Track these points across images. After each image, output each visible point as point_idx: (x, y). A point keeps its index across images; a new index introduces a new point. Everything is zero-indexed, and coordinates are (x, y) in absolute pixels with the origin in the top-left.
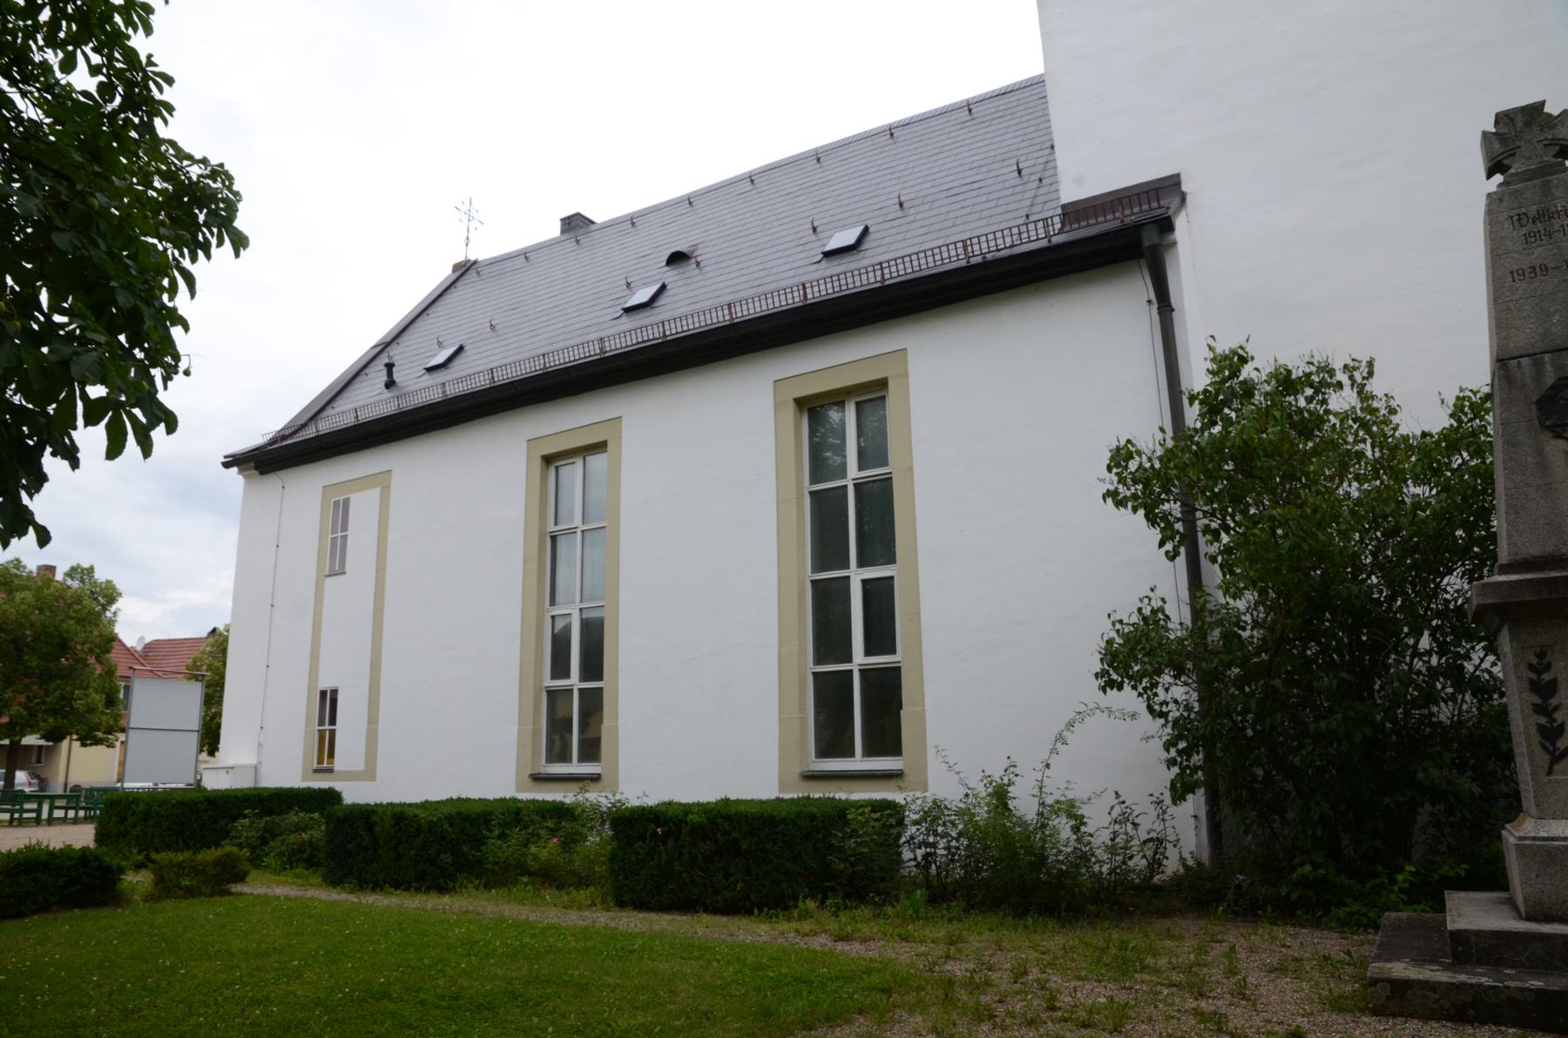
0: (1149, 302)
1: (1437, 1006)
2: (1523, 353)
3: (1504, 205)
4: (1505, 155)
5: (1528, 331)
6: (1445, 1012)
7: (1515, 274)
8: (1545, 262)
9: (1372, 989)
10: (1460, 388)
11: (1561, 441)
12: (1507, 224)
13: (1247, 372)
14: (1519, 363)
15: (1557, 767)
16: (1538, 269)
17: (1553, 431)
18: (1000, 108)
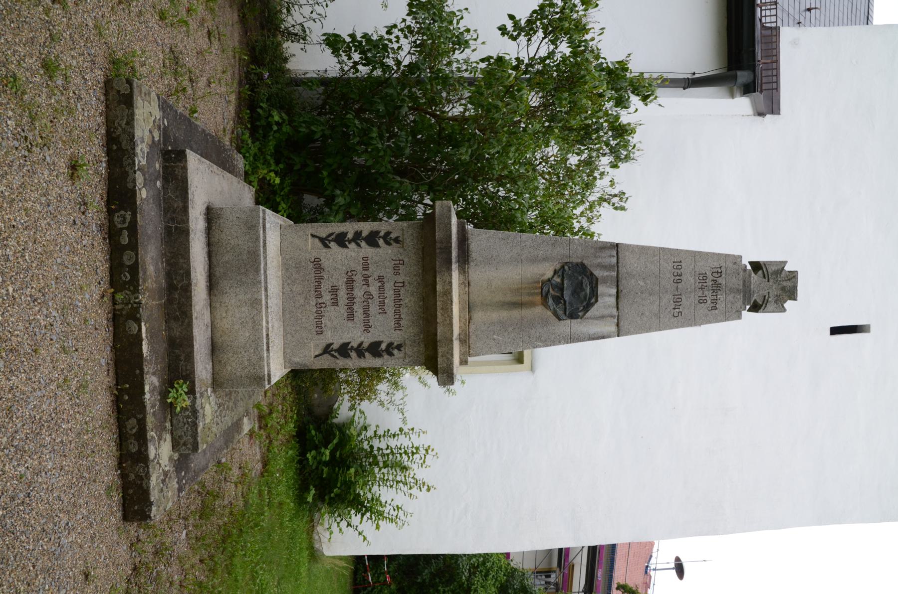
0: (694, 74)
1: (116, 125)
2: (620, 260)
3: (731, 265)
4: (766, 272)
5: (636, 265)
6: (112, 130)
7: (679, 264)
8: (683, 283)
9: (125, 81)
10: (601, 235)
11: (552, 273)
12: (716, 264)
13: (635, 100)
14: (614, 256)
15: (317, 240)
16: (679, 278)
17: (560, 270)
18: (858, 12)
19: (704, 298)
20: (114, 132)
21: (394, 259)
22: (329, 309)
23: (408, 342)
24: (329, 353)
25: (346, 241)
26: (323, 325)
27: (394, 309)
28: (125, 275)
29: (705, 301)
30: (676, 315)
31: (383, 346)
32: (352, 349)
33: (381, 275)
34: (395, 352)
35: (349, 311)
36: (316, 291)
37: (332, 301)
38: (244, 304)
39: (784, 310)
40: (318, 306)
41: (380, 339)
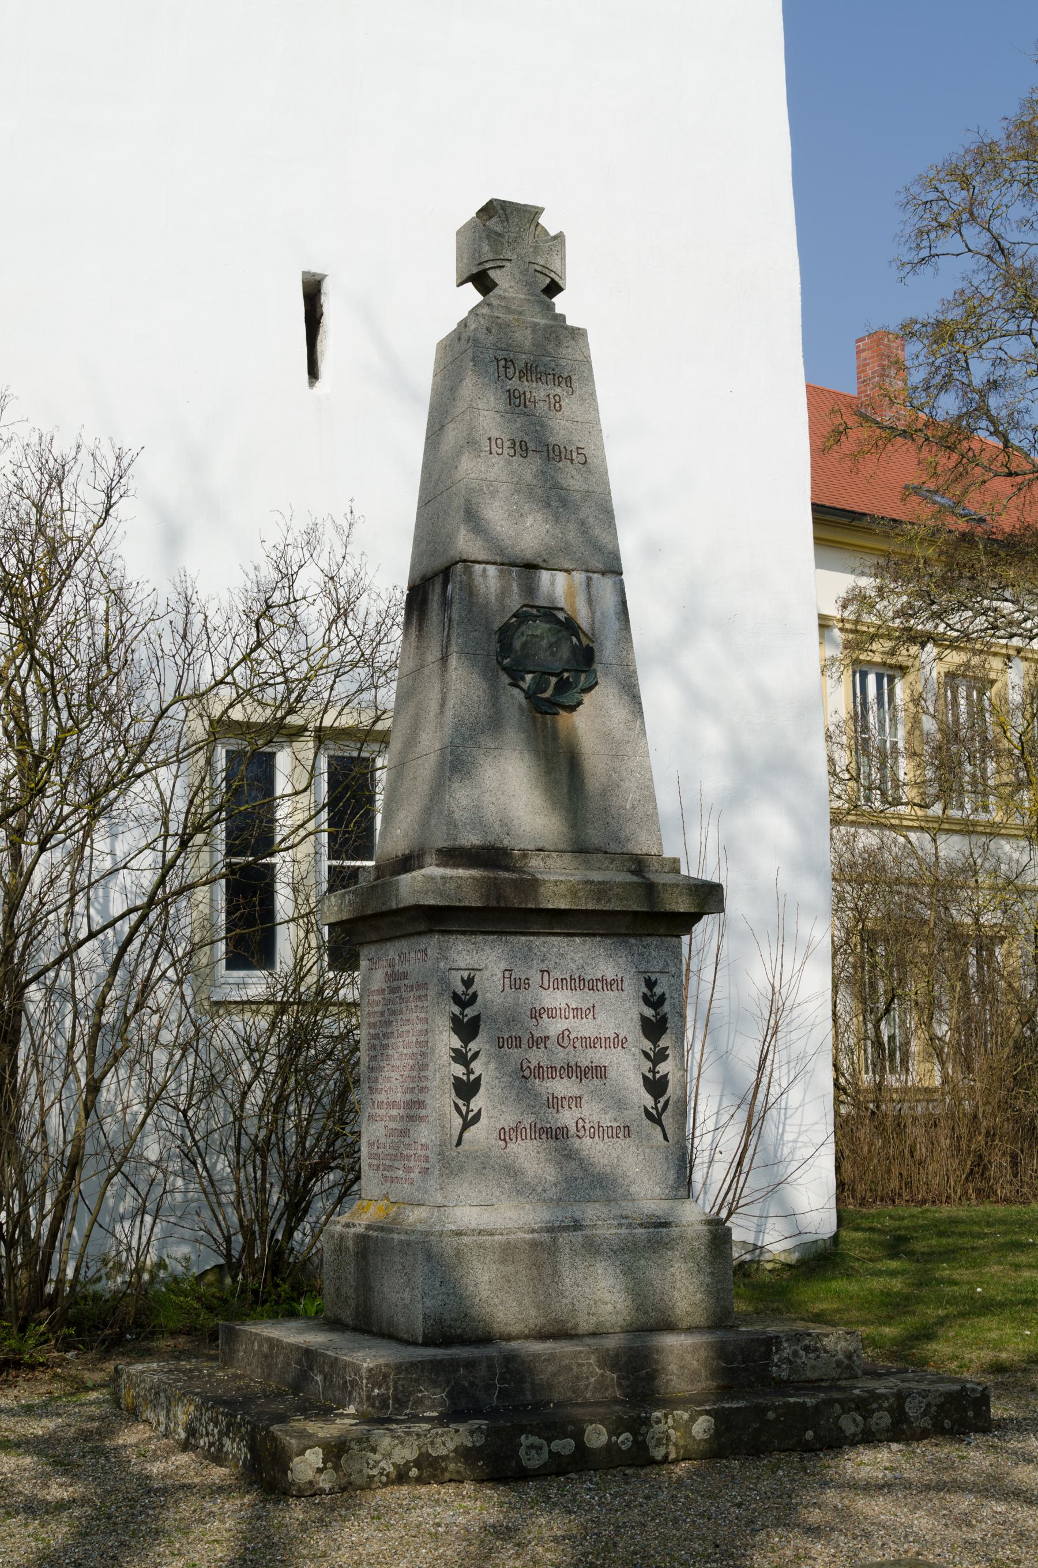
7: (493, 442)
8: (526, 439)
19: (553, 401)
20: (387, 1475)
21: (501, 988)
22: (587, 1114)
23: (643, 967)
24: (660, 1115)
25: (468, 1078)
26: (615, 1125)
27: (586, 990)
28: (623, 1443)
29: (557, 398)
30: (582, 459)
31: (649, 1012)
32: (653, 1071)
33: (529, 1013)
34: (658, 990)
35: (590, 1074)
36: (557, 1139)
37: (573, 1106)
38: (591, 1269)
39: (560, 237)
40: (581, 1134)
41: (636, 1017)
